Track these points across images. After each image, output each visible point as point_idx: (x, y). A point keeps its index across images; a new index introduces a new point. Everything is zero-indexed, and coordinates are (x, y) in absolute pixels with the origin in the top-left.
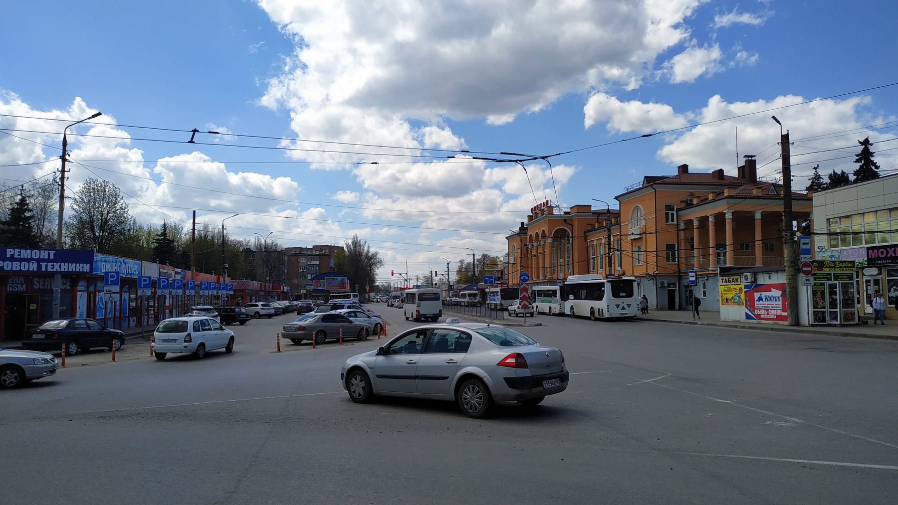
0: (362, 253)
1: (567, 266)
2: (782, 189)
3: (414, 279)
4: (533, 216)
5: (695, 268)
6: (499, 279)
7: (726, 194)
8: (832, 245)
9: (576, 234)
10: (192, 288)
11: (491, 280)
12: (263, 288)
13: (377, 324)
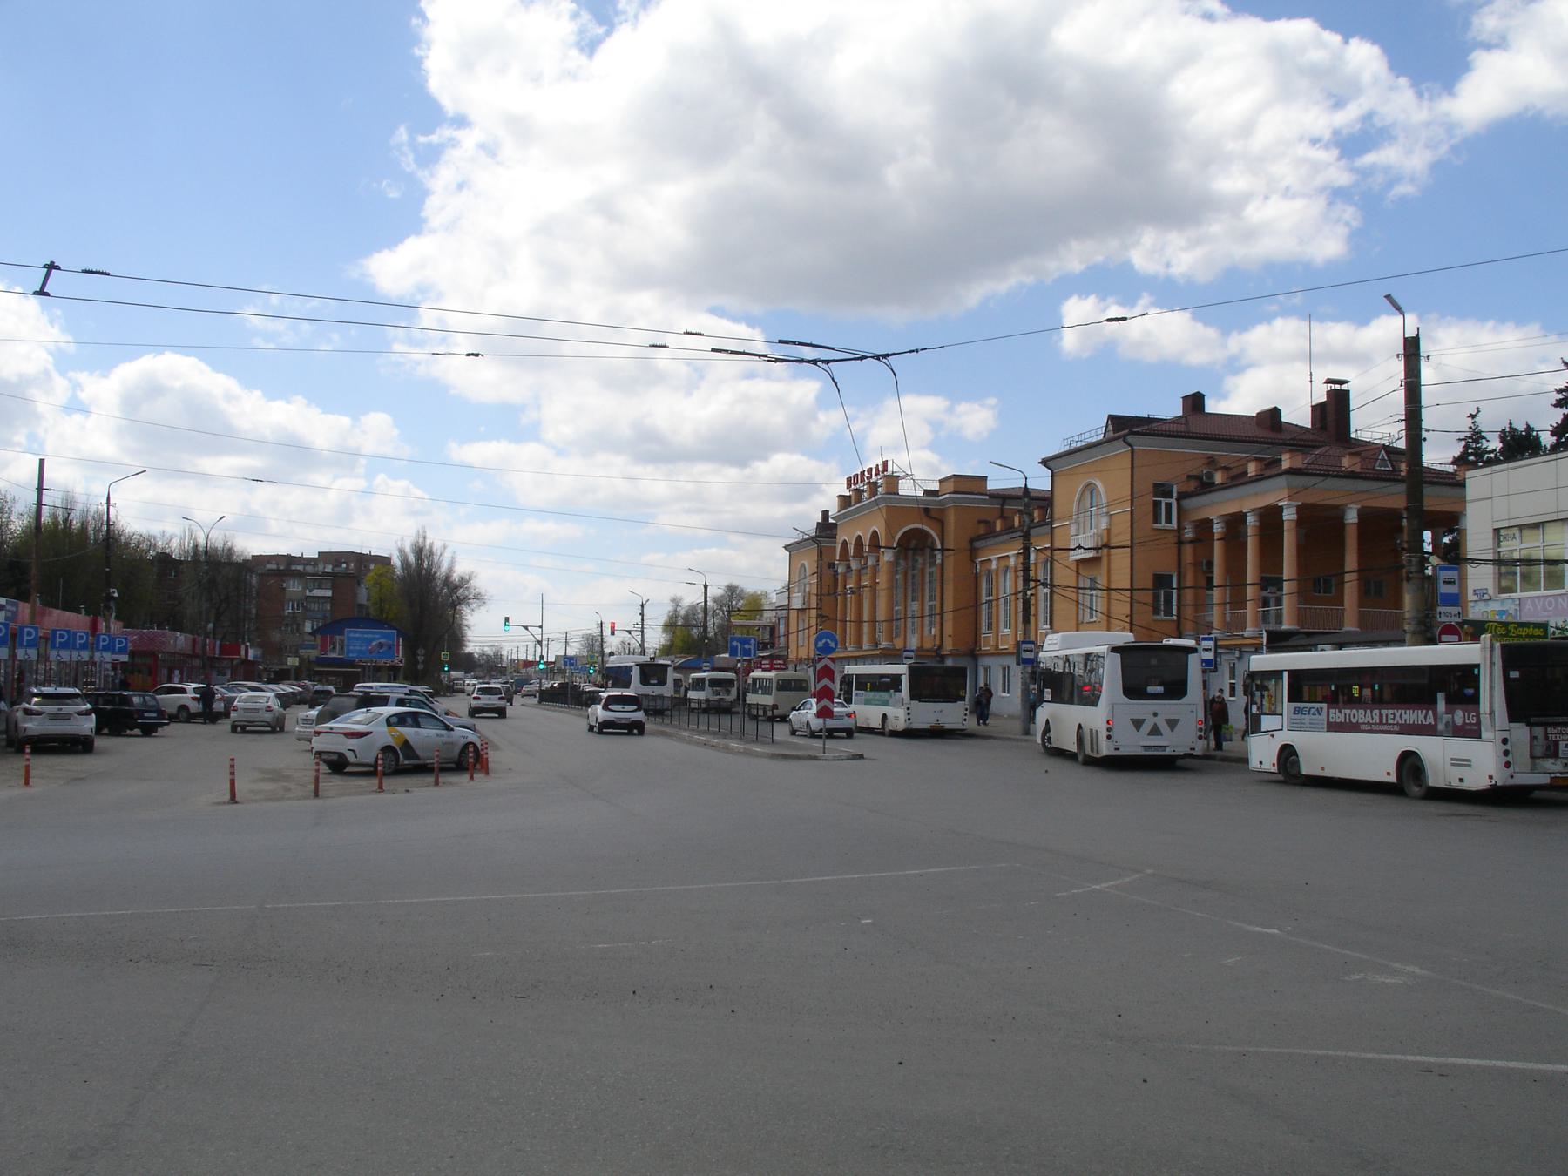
0: (435, 573)
1: (926, 620)
2: (1403, 458)
3: (558, 640)
4: (850, 496)
5: (1214, 631)
6: (765, 646)
7: (1286, 465)
8: (1504, 588)
9: (950, 544)
10: (31, 644)
11: (747, 647)
12: (199, 650)
13: (467, 745)
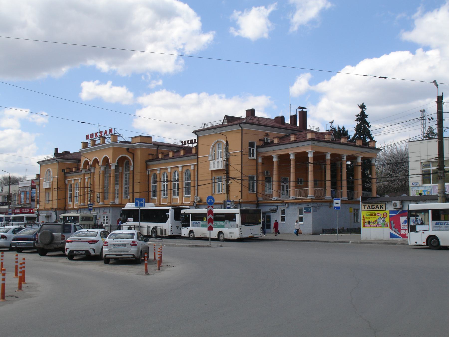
11: (141, 202)
